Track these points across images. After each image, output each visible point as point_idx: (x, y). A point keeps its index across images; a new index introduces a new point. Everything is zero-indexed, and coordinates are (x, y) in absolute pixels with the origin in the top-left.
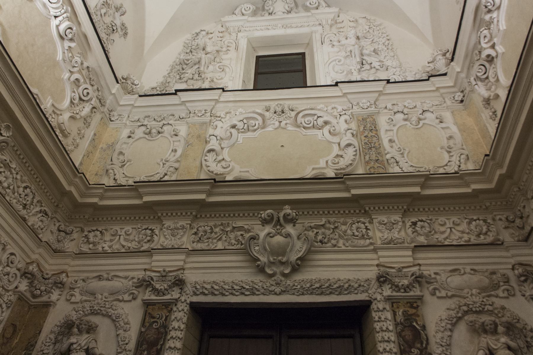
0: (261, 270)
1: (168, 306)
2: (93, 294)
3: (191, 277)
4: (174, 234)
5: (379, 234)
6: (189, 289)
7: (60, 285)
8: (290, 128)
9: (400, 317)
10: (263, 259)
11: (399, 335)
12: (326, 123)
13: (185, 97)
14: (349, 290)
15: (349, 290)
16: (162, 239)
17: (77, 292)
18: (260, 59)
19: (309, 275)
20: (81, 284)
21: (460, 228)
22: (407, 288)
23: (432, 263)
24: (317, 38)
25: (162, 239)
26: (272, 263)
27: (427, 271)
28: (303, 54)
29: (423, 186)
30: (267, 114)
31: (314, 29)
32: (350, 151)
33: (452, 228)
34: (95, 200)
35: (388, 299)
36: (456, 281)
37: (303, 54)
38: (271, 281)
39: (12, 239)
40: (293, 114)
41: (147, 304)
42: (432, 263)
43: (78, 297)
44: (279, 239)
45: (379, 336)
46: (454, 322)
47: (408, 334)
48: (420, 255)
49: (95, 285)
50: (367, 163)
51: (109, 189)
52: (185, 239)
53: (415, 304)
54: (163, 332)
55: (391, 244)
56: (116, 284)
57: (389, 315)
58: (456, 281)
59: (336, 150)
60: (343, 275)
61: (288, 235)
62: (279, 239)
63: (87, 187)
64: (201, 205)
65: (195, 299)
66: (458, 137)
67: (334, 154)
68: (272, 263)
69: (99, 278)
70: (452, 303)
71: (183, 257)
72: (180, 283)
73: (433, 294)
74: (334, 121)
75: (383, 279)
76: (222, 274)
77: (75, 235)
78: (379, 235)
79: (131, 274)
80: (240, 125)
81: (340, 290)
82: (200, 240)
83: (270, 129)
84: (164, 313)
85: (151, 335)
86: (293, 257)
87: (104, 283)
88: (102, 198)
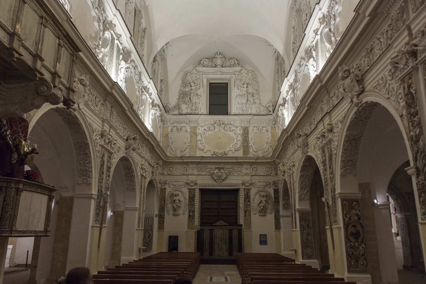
0: (215, 180)
1: (194, 189)
2: (175, 186)
3: (199, 182)
4: (193, 170)
5: (244, 171)
6: (198, 185)
7: (166, 183)
8: (223, 131)
9: (245, 193)
10: (216, 178)
11: (245, 197)
12: (233, 130)
13: (188, 116)
14: (236, 186)
15: (236, 186)
16: (190, 171)
17: (171, 185)
18: (212, 85)
19: (227, 182)
20: (171, 183)
21: (263, 170)
22: (248, 186)
23: (255, 179)
24: (233, 81)
25: (190, 171)
26: (218, 179)
27: (253, 181)
28: (227, 83)
29: (256, 160)
30: (215, 125)
31: (232, 75)
32: (240, 142)
33: (262, 170)
34: (171, 161)
35: (243, 189)
36: (259, 184)
37: (227, 83)
38: (218, 183)
39: (95, 122)
40: (224, 126)
41: (189, 189)
42: (255, 179)
43: (171, 187)
44: (220, 173)
45: (240, 197)
46: (257, 194)
47: (246, 197)
48: (252, 177)
49: (175, 183)
50: (244, 147)
51: (174, 157)
52: (195, 171)
53: (249, 190)
54: (194, 195)
55: (246, 174)
56: (180, 183)
57: (243, 192)
58: (259, 184)
59: (235, 142)
60: (235, 182)
61: (222, 173)
62: (220, 173)
63: (168, 157)
64: (199, 162)
65: (200, 187)
66: (270, 139)
67: (235, 143)
68: (218, 179)
69: (176, 182)
70: (257, 189)
71: (196, 177)
72: (196, 184)
73: (254, 187)
74: (236, 129)
75: (243, 184)
76: (205, 181)
77: (166, 169)
78: (244, 171)
79: (184, 180)
80: (207, 129)
81: (233, 186)
82: (199, 171)
83: (216, 130)
84: (194, 191)
85: (192, 196)
86: (223, 178)
87: (177, 183)
88: (172, 160)
